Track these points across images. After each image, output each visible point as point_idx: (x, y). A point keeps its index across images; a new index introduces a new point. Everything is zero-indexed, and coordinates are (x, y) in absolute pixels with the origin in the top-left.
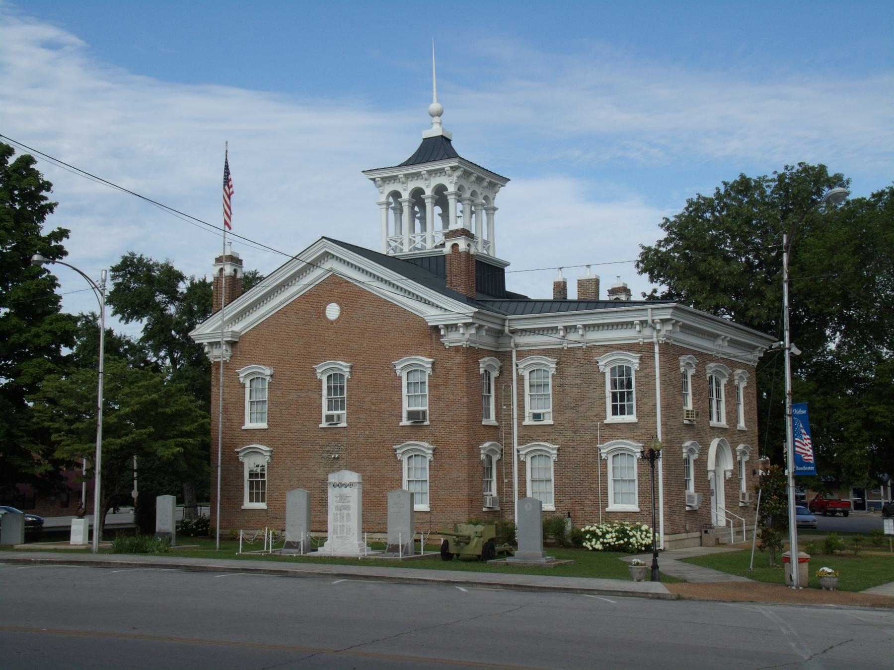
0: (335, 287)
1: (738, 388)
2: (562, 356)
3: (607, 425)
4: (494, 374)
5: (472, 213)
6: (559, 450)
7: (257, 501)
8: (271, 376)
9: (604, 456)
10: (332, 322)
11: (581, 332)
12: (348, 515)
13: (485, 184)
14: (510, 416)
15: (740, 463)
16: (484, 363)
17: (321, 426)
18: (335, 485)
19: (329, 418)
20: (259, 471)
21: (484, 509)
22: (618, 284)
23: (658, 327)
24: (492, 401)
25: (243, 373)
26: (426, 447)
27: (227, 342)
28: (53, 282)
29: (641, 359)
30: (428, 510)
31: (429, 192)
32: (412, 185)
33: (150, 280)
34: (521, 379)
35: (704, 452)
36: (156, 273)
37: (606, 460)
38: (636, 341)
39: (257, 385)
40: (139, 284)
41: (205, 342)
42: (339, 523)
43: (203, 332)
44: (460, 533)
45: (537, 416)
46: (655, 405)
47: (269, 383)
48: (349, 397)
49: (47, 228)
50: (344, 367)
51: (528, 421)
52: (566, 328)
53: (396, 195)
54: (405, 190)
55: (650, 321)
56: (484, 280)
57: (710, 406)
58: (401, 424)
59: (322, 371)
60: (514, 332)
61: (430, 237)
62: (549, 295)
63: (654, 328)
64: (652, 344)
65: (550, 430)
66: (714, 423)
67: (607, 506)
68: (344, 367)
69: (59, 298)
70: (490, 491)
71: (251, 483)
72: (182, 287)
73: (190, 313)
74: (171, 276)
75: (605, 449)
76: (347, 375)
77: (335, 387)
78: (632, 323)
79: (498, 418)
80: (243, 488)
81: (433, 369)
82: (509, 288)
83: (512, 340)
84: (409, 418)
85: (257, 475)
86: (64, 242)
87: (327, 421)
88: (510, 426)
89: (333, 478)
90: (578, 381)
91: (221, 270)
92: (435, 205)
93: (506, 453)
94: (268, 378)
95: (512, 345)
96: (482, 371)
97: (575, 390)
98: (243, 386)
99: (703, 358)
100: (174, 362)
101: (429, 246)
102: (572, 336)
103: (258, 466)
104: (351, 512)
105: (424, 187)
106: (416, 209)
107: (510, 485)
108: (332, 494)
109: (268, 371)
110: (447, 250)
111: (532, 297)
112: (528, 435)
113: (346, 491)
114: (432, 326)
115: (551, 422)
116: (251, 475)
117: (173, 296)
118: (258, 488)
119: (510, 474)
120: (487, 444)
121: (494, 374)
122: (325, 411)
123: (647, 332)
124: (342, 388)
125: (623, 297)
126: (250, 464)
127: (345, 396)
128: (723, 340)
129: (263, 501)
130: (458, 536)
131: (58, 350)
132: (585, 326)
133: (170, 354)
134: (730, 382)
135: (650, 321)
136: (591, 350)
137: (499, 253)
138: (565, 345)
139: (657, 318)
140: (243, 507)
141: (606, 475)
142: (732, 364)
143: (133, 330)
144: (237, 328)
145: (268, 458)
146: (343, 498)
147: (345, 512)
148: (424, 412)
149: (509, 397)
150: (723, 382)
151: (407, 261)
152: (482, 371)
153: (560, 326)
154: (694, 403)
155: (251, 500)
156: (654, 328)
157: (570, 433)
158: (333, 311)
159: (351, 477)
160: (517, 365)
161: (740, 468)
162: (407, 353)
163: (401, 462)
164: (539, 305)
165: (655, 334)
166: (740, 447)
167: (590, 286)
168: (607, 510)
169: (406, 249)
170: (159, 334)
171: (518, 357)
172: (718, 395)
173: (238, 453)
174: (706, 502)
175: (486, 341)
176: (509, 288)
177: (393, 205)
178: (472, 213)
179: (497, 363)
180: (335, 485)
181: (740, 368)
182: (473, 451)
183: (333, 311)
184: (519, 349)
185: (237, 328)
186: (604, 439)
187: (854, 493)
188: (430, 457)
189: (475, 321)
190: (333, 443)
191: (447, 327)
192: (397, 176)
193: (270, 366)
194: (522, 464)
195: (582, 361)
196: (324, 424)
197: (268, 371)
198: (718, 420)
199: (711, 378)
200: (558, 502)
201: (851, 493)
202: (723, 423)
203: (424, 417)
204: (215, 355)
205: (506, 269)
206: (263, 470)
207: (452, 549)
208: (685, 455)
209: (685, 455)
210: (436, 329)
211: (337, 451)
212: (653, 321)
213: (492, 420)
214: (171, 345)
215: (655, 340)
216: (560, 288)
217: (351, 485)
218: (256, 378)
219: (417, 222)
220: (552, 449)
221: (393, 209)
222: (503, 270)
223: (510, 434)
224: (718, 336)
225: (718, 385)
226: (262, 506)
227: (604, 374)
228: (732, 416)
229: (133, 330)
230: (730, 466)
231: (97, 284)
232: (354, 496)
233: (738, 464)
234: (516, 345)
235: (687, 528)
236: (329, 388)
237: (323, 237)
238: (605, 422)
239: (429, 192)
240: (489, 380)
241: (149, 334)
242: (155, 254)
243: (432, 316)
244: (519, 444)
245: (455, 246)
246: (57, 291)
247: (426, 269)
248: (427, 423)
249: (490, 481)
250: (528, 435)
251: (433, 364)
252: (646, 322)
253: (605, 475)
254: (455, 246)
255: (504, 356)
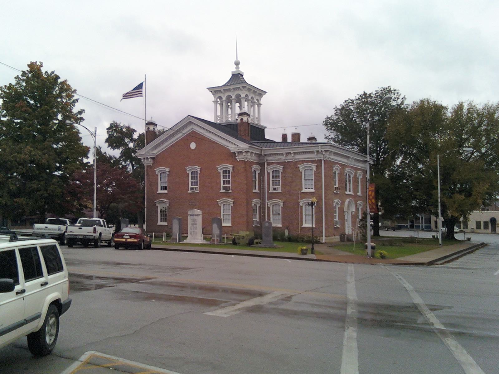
0: (194, 136)
1: (358, 179)
2: (285, 165)
3: (303, 193)
4: (258, 172)
5: (251, 106)
6: (283, 202)
7: (164, 222)
8: (169, 172)
9: (301, 205)
10: (193, 150)
11: (292, 155)
12: (196, 227)
13: (257, 94)
14: (264, 188)
15: (358, 209)
16: (254, 167)
17: (188, 192)
18: (191, 215)
19: (192, 189)
20: (164, 210)
21: (254, 226)
22: (311, 136)
23: (324, 153)
24: (257, 182)
25: (158, 170)
26: (230, 201)
27: (151, 158)
28: (78, 133)
29: (317, 166)
30: (231, 225)
31: (233, 97)
32: (227, 94)
33: (121, 132)
34: (268, 174)
35: (343, 203)
36: (124, 130)
37: (302, 207)
38: (315, 159)
39: (163, 175)
40: (118, 135)
41: (142, 158)
42: (192, 230)
43: (141, 153)
44: (240, 235)
45: (275, 189)
46: (322, 185)
47: (168, 175)
48: (200, 181)
49: (75, 110)
50: (198, 168)
51: (271, 191)
52: (287, 154)
53: (221, 98)
54: (233, 95)
55: (320, 151)
56: (256, 134)
57: (346, 186)
58: (220, 191)
59: (189, 170)
60: (265, 155)
61: (232, 116)
62: (279, 140)
63: (322, 154)
64: (321, 160)
65: (280, 194)
66: (347, 192)
67: (302, 225)
68: (198, 168)
69: (81, 138)
70: (256, 218)
71: (161, 214)
72: (135, 136)
73: (138, 146)
74: (130, 131)
75: (302, 202)
76: (199, 172)
77: (194, 176)
78: (313, 152)
79: (259, 189)
80: (158, 217)
81: (233, 170)
82: (266, 137)
83: (265, 158)
84: (223, 189)
85: (163, 211)
86: (83, 115)
87: (191, 190)
88: (264, 193)
89: (190, 212)
90: (291, 175)
91: (148, 128)
92: (236, 103)
93: (263, 203)
94: (167, 173)
95: (265, 160)
96: (253, 171)
97: (290, 178)
98: (158, 175)
99: (343, 166)
100: (133, 166)
101: (234, 119)
102: (289, 157)
103: (164, 208)
104: (197, 226)
105: (232, 96)
106: (229, 104)
107: (264, 216)
108: (190, 219)
109: (167, 170)
110: (239, 121)
111: (276, 141)
112: (271, 196)
113: (195, 217)
114: (232, 152)
115: (281, 191)
116: (161, 211)
117: (132, 140)
118: (164, 217)
119: (264, 212)
120: (254, 200)
121: (258, 172)
122: (190, 186)
123: (320, 155)
124: (197, 177)
125: (314, 141)
126: (160, 207)
127: (198, 180)
128: (352, 159)
129: (166, 222)
130: (239, 236)
131: (82, 160)
132: (294, 153)
133: (131, 162)
134: (356, 175)
135: (320, 151)
136: (296, 163)
137: (263, 123)
138: (286, 161)
139: (323, 150)
140: (158, 224)
141: (302, 213)
142: (356, 169)
143: (116, 153)
144: (155, 152)
145: (168, 205)
146: (194, 220)
147: (195, 226)
148: (229, 187)
149: (264, 181)
150: (352, 176)
151: (225, 125)
152: (253, 171)
153: (284, 153)
154: (338, 184)
155: (161, 221)
156: (322, 154)
157: (288, 196)
158: (193, 146)
159: (200, 212)
160: (267, 168)
161: (358, 211)
162: (222, 163)
163: (220, 207)
164: (276, 144)
165: (322, 156)
166: (359, 202)
167: (297, 137)
168: (302, 226)
169: (224, 121)
170: (127, 154)
171: (268, 165)
172: (350, 181)
173: (156, 202)
174: (343, 225)
175: (254, 159)
176: (266, 137)
177: (219, 102)
178: (251, 106)
179: (258, 167)
180: (191, 215)
181: (359, 171)
182: (248, 203)
183: (193, 146)
184: (268, 162)
185: (155, 152)
186: (301, 198)
187: (410, 221)
188: (232, 205)
189: (249, 150)
190: (193, 199)
191: (238, 152)
192: (230, 89)
193: (168, 168)
194: (269, 208)
195: (293, 167)
196: (190, 191)
197: (167, 170)
198: (350, 191)
199: (346, 174)
200: (283, 223)
201: (409, 221)
202: (351, 193)
203: (229, 189)
204: (146, 163)
205: (265, 130)
206: (166, 209)
207: (237, 241)
208: (334, 205)
209: (334, 205)
210: (234, 153)
211: (194, 201)
212: (321, 151)
213: (257, 191)
214: (132, 159)
215: (322, 158)
216: (284, 137)
217: (198, 215)
218: (163, 173)
219: (229, 110)
220: (281, 202)
221: (219, 104)
222: (264, 130)
223: (264, 195)
224: (349, 157)
225: (350, 177)
226: (166, 224)
227: (302, 172)
228: (355, 190)
229: (116, 153)
230: (354, 210)
231: (93, 133)
232: (199, 220)
233: (357, 209)
234: (267, 160)
235: (335, 234)
236: (192, 177)
237: (189, 115)
238: (302, 191)
239: (233, 97)
240: (256, 174)
241: (123, 154)
242: (123, 122)
243: (232, 148)
244: (268, 200)
245: (242, 119)
246: (80, 135)
247: (231, 129)
248: (230, 191)
249: (256, 215)
250: (271, 196)
251: (233, 167)
252: (318, 151)
253: (301, 213)
254: (242, 119)
255: (262, 165)
